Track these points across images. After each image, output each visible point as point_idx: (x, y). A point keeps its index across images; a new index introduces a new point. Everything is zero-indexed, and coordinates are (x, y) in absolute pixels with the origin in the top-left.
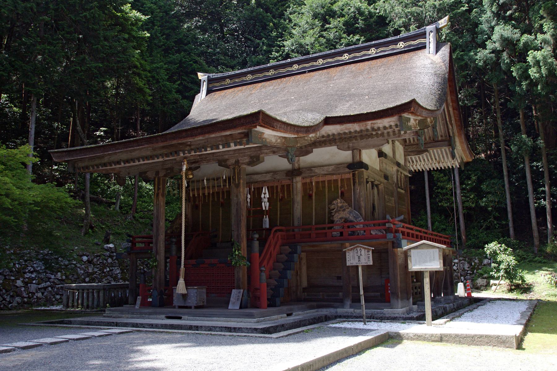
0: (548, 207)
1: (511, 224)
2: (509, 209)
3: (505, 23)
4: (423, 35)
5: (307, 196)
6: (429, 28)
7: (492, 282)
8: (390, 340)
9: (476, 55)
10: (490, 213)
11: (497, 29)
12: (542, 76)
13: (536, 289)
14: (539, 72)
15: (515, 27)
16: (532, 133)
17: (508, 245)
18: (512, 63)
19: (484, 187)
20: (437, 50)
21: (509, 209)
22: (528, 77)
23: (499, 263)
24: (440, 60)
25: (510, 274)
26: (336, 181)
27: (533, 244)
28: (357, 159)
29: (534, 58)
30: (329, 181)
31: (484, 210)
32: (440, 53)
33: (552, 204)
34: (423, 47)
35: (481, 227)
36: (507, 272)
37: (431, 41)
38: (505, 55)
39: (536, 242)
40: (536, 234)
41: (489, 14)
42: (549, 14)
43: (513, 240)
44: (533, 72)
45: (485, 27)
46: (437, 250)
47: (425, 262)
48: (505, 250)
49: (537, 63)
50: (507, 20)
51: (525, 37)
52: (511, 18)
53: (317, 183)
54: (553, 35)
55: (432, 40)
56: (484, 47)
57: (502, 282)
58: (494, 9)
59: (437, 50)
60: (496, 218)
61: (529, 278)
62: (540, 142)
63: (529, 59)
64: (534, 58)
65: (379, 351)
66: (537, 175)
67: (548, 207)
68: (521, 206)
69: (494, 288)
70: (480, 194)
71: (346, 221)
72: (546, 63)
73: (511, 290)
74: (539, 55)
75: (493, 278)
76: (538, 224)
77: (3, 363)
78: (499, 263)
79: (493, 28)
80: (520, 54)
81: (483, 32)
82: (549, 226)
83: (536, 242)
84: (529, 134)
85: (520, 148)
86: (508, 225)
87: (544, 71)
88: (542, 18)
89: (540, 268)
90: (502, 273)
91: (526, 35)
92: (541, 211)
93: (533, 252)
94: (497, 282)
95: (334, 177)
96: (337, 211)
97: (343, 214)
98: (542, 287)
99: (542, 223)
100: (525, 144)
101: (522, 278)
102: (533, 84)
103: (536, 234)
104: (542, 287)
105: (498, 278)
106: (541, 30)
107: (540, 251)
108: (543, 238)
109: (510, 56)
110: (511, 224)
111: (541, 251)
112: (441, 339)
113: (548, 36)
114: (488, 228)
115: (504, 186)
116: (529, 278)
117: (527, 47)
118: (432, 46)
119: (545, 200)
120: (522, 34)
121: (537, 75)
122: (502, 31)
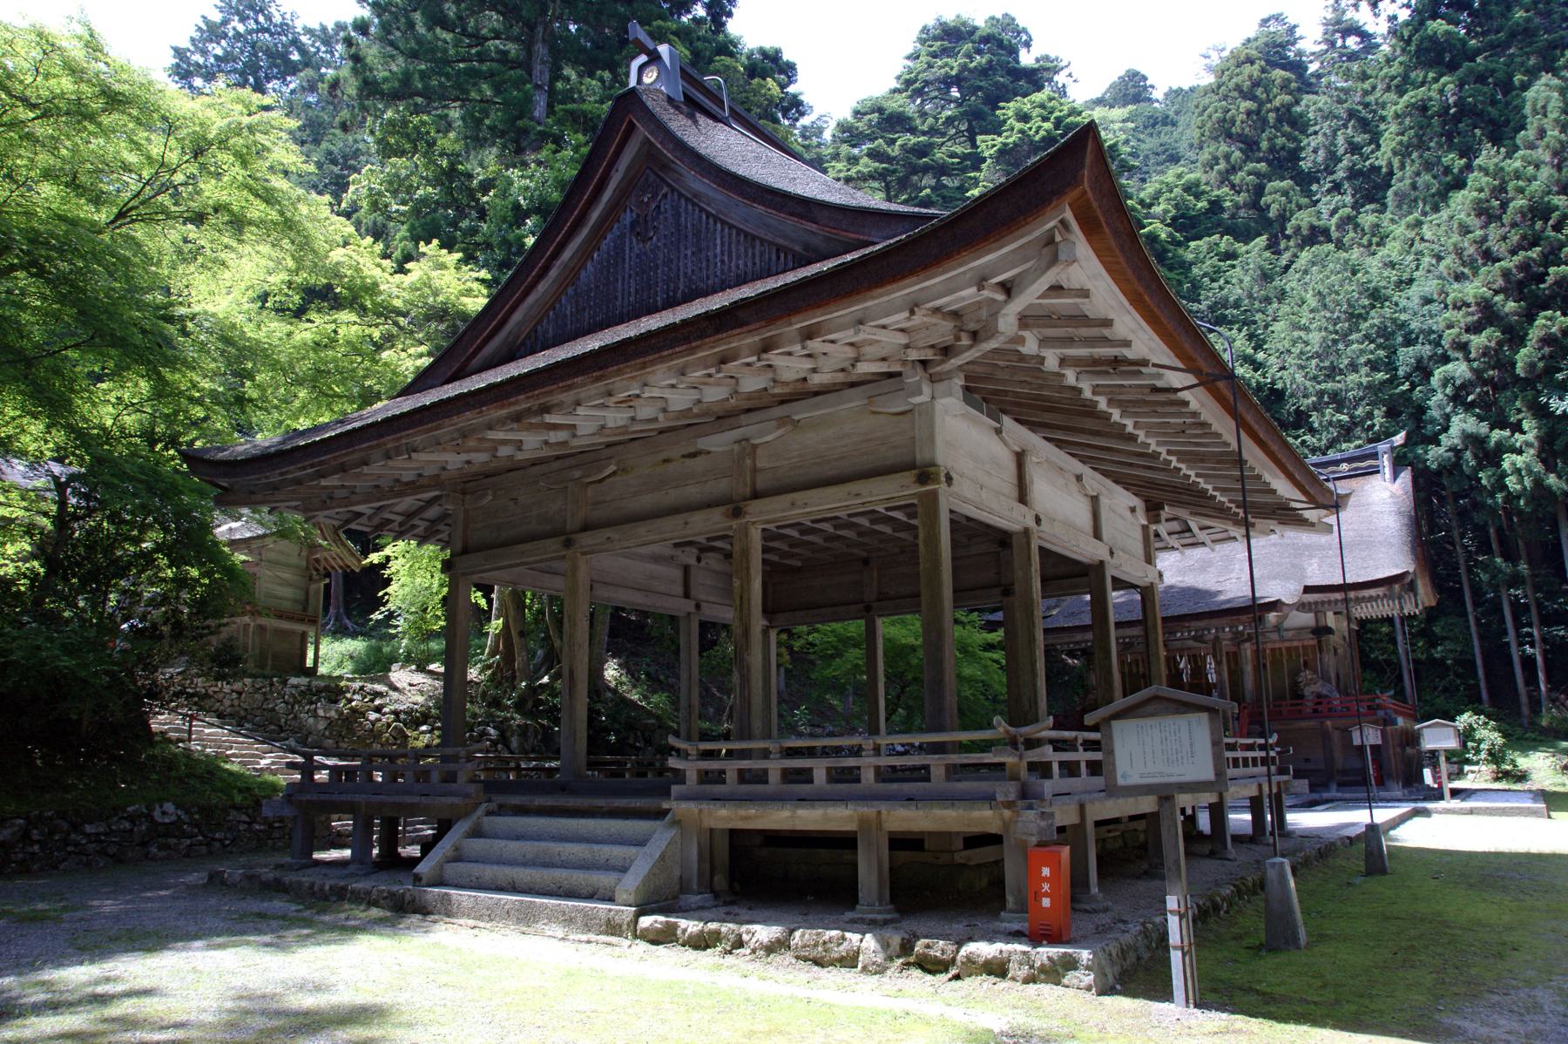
0: (1539, 659)
1: (1483, 684)
2: (1479, 662)
3: (1466, 411)
4: (1375, 456)
5: (1259, 667)
6: (1382, 447)
7: (1467, 768)
8: (1425, 813)
9: (1426, 452)
10: (1447, 668)
11: (1455, 420)
12: (1525, 488)
13: (1534, 777)
14: (1521, 481)
15: (1481, 419)
16: (1511, 556)
17: (1488, 716)
18: (1480, 467)
19: (1437, 629)
20: (1395, 477)
21: (1479, 662)
22: (1504, 487)
23: (1480, 741)
24: (1400, 492)
25: (1495, 757)
26: (1297, 648)
27: (1519, 714)
28: (1322, 623)
29: (1513, 464)
30: (1288, 649)
31: (1441, 662)
32: (1399, 481)
33: (1545, 653)
34: (1375, 471)
35: (1435, 688)
36: (1490, 753)
37: (1386, 462)
38: (1468, 455)
39: (1525, 710)
40: (1524, 699)
41: (1440, 396)
42: (1530, 408)
43: (1486, 706)
44: (1511, 482)
45: (1435, 413)
46: (1204, 716)
47: (1439, 740)
48: (1486, 724)
49: (1518, 471)
50: (1469, 407)
51: (1497, 435)
52: (1472, 405)
53: (1273, 650)
54: (1537, 437)
55: (1386, 463)
56: (1438, 444)
57: (1484, 768)
58: (1448, 391)
59: (1395, 477)
60: (1458, 675)
61: (1523, 762)
62: (1523, 567)
63: (1506, 465)
64: (1513, 464)
65: (1417, 820)
66: (1519, 610)
67: (1539, 659)
68: (1497, 654)
69: (1470, 776)
70: (1433, 642)
71: (1319, 696)
72: (1530, 472)
73: (1497, 779)
74: (1520, 460)
75: (1468, 762)
76: (1527, 683)
77: (9, 1034)
78: (1480, 741)
79: (1447, 418)
80: (1491, 457)
81: (1432, 421)
82: (1543, 687)
83: (1525, 710)
84: (1506, 558)
85: (1493, 577)
86: (1478, 685)
87: (1528, 482)
88: (1519, 411)
89: (1535, 749)
90: (1483, 755)
91: (1497, 431)
92: (1528, 662)
93: (1521, 725)
94: (1475, 768)
95: (1295, 644)
96: (1307, 684)
97: (1314, 688)
98: (1542, 774)
99: (1531, 680)
100: (1500, 571)
101: (1513, 761)
102: (1511, 498)
103: (1524, 699)
104: (1542, 774)
105: (1477, 763)
106: (1517, 428)
107: (1532, 723)
108: (1535, 705)
109: (1475, 456)
110: (1483, 684)
111: (1534, 725)
112: (1471, 812)
113: (1530, 437)
114: (1445, 690)
115: (1468, 628)
116: (1523, 762)
117: (1501, 449)
118: (1388, 471)
119: (1532, 646)
120: (1492, 429)
121: (1518, 487)
122: (1463, 423)
